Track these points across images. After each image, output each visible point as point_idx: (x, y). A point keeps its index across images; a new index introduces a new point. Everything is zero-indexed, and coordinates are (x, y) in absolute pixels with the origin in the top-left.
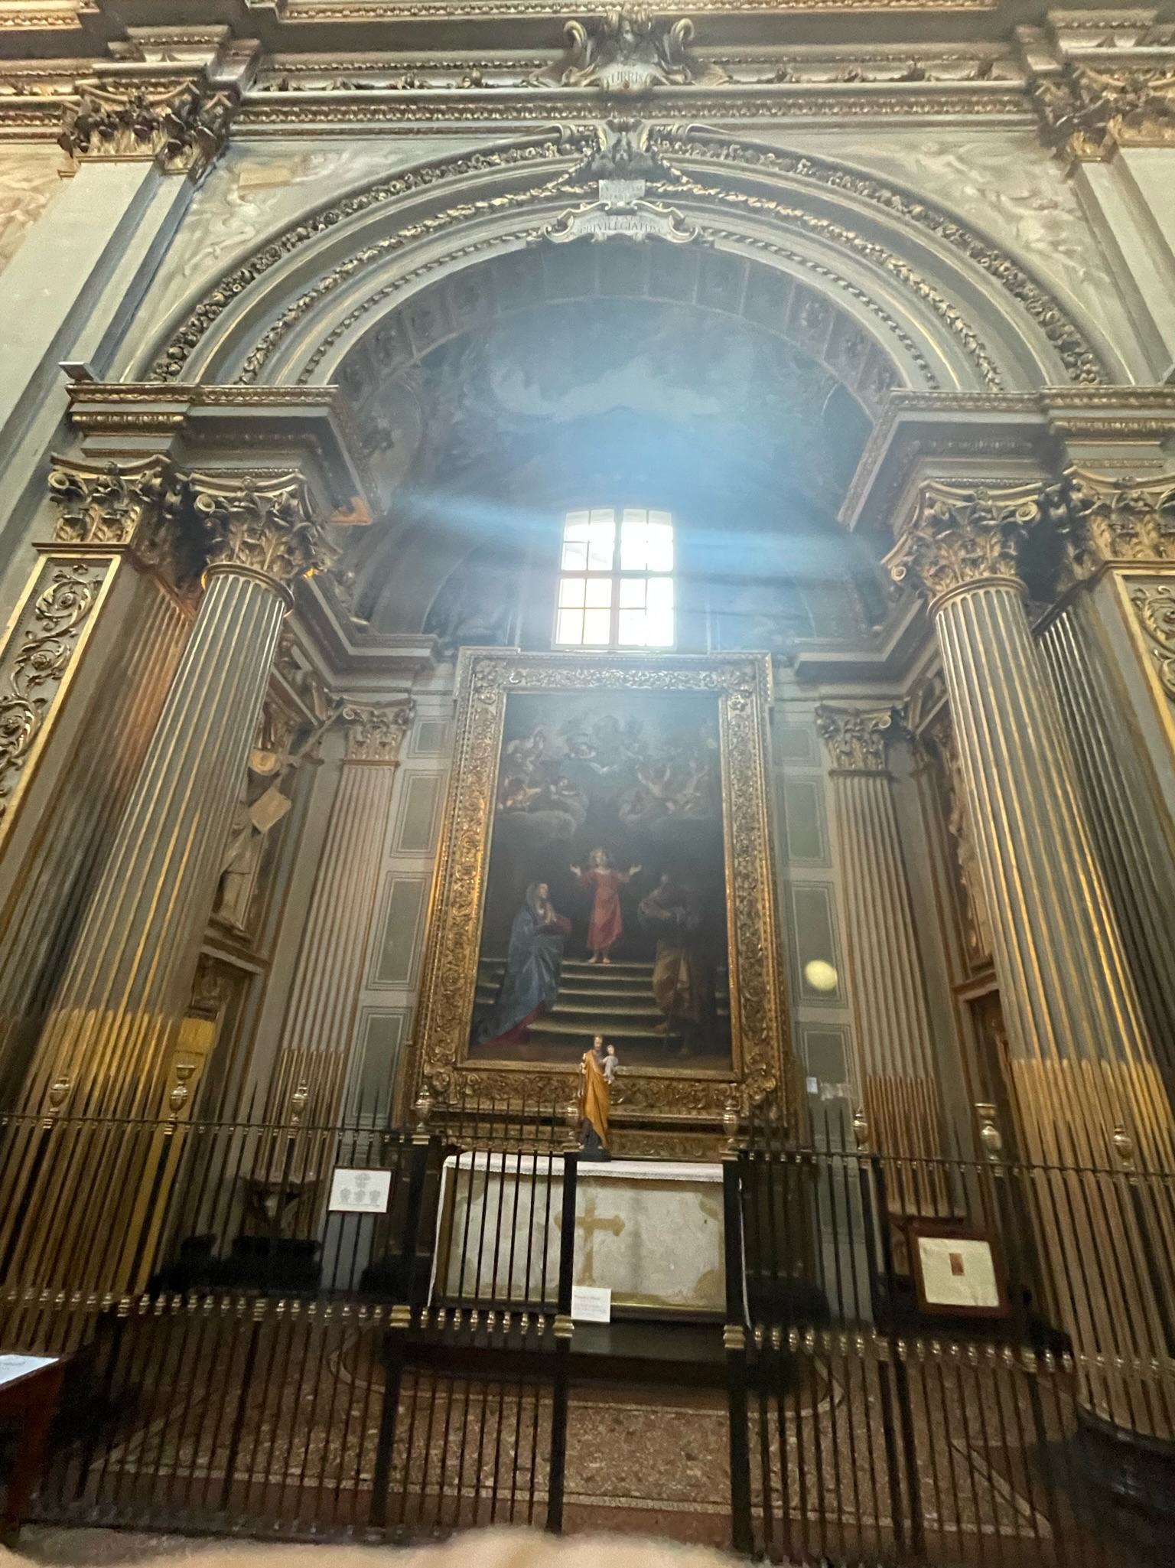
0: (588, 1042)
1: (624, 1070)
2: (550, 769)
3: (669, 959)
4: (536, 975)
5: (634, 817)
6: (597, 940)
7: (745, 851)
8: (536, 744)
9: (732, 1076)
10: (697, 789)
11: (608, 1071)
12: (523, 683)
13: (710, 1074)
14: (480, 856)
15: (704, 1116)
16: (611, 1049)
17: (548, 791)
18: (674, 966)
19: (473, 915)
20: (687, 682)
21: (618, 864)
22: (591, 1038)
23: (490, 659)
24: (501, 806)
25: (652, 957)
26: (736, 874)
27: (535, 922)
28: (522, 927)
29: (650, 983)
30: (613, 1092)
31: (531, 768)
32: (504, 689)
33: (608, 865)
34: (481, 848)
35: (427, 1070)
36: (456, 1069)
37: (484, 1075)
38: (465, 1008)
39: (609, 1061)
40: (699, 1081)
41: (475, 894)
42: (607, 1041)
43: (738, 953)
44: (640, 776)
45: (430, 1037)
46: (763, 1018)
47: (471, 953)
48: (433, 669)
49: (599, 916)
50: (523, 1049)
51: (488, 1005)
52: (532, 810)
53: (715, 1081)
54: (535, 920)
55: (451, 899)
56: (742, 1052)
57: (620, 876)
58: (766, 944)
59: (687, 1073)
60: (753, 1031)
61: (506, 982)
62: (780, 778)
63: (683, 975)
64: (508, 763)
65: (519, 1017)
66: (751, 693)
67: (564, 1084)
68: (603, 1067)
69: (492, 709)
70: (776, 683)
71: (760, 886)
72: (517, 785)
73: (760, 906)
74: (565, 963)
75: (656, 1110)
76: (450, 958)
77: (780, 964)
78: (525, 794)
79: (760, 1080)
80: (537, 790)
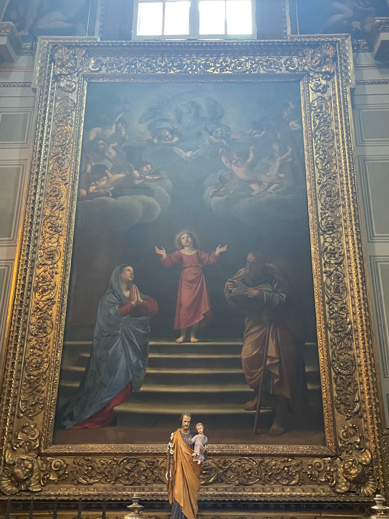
0: (176, 421)
1: (215, 448)
2: (132, 155)
3: (257, 336)
4: (123, 357)
5: (217, 199)
6: (183, 317)
7: (331, 228)
8: (118, 130)
9: (323, 450)
10: (281, 170)
11: (197, 451)
12: (104, 71)
13: (304, 449)
14: (62, 241)
15: (298, 492)
16: (200, 427)
17: (131, 177)
18: (262, 343)
19: (57, 300)
20: (268, 67)
21: (201, 245)
22: (179, 417)
23: (69, 46)
24: (84, 192)
25: (240, 334)
26: (323, 251)
27: (121, 305)
28: (107, 309)
29: (240, 359)
30: (203, 471)
31: (114, 153)
32: (85, 77)
33: (194, 245)
34: (64, 233)
35: (9, 457)
36: (40, 454)
37: (69, 461)
38: (49, 393)
39: (199, 440)
40: (292, 456)
41: (58, 279)
42: (195, 419)
43: (327, 327)
44: (223, 160)
45: (12, 424)
46: (355, 391)
47: (55, 338)
48: (12, 61)
49: (186, 296)
50: (110, 431)
51: (75, 388)
52: (115, 195)
53: (305, 456)
54: (122, 301)
55: (34, 284)
56: (334, 426)
57: (204, 255)
58: (354, 315)
59: (281, 449)
60: (345, 403)
61: (93, 367)
62: (363, 159)
63: (272, 351)
64: (89, 149)
65: (105, 397)
66: (332, 75)
67: (153, 466)
68: (192, 446)
69: (73, 97)
70: (357, 66)
71: (346, 262)
72: (100, 171)
73: (347, 280)
74: (151, 343)
75: (248, 488)
76: (33, 343)
77: (370, 337)
78: (108, 179)
79: (355, 453)
80: (121, 175)
